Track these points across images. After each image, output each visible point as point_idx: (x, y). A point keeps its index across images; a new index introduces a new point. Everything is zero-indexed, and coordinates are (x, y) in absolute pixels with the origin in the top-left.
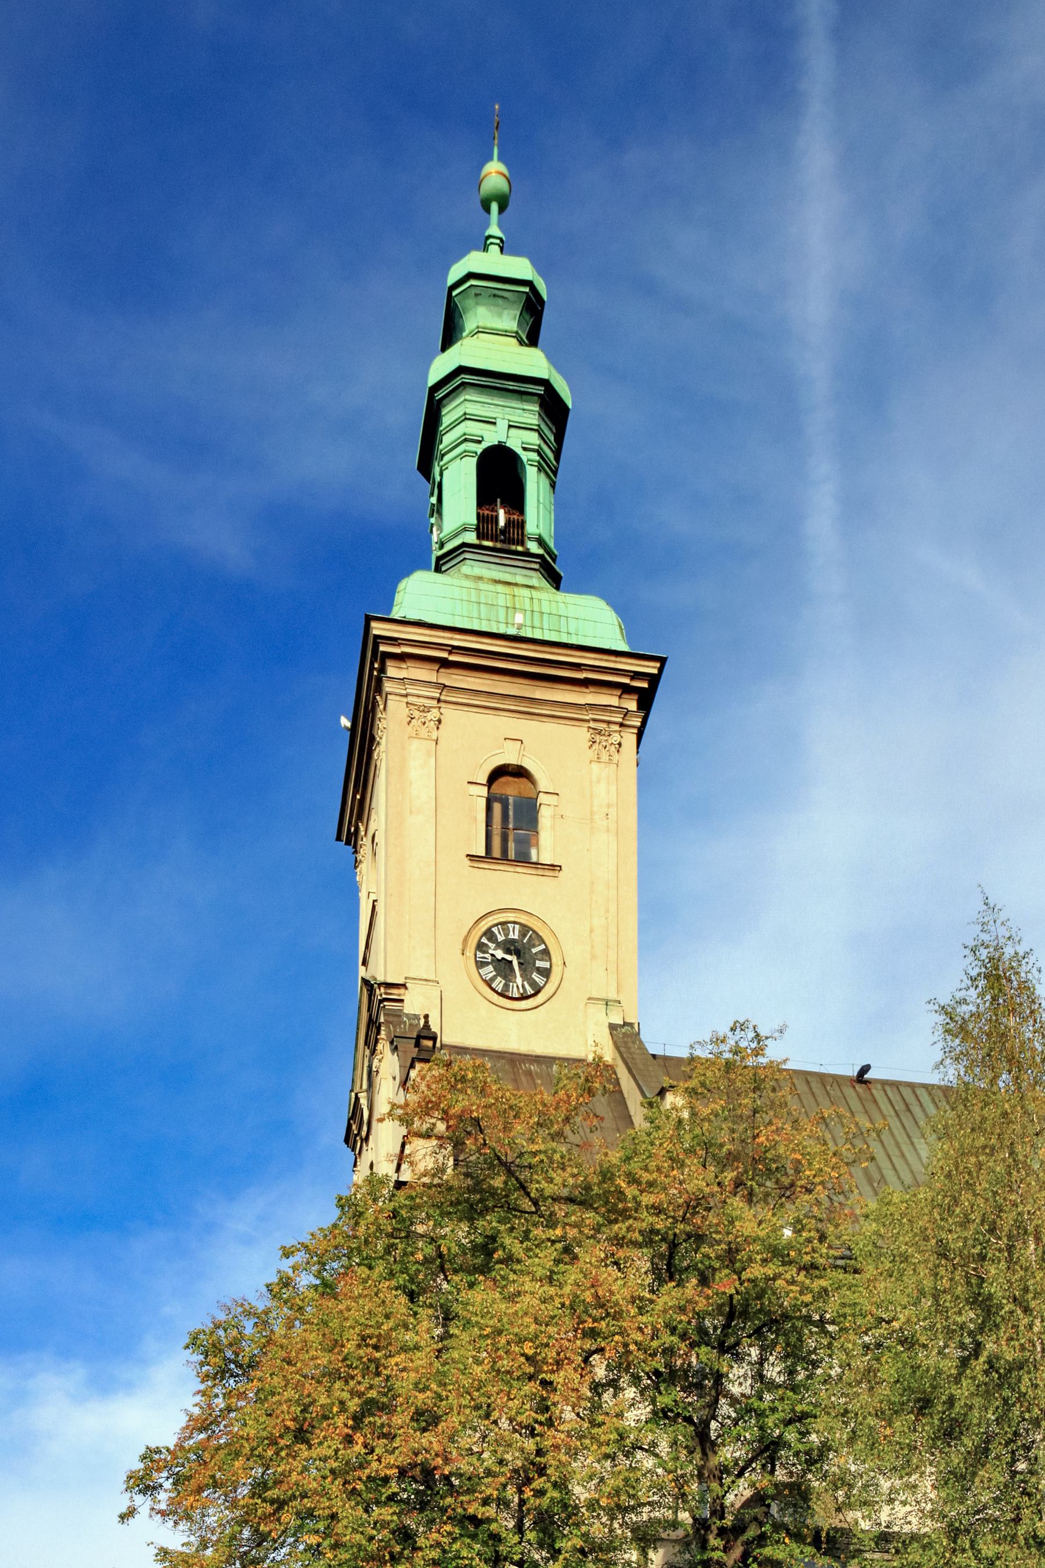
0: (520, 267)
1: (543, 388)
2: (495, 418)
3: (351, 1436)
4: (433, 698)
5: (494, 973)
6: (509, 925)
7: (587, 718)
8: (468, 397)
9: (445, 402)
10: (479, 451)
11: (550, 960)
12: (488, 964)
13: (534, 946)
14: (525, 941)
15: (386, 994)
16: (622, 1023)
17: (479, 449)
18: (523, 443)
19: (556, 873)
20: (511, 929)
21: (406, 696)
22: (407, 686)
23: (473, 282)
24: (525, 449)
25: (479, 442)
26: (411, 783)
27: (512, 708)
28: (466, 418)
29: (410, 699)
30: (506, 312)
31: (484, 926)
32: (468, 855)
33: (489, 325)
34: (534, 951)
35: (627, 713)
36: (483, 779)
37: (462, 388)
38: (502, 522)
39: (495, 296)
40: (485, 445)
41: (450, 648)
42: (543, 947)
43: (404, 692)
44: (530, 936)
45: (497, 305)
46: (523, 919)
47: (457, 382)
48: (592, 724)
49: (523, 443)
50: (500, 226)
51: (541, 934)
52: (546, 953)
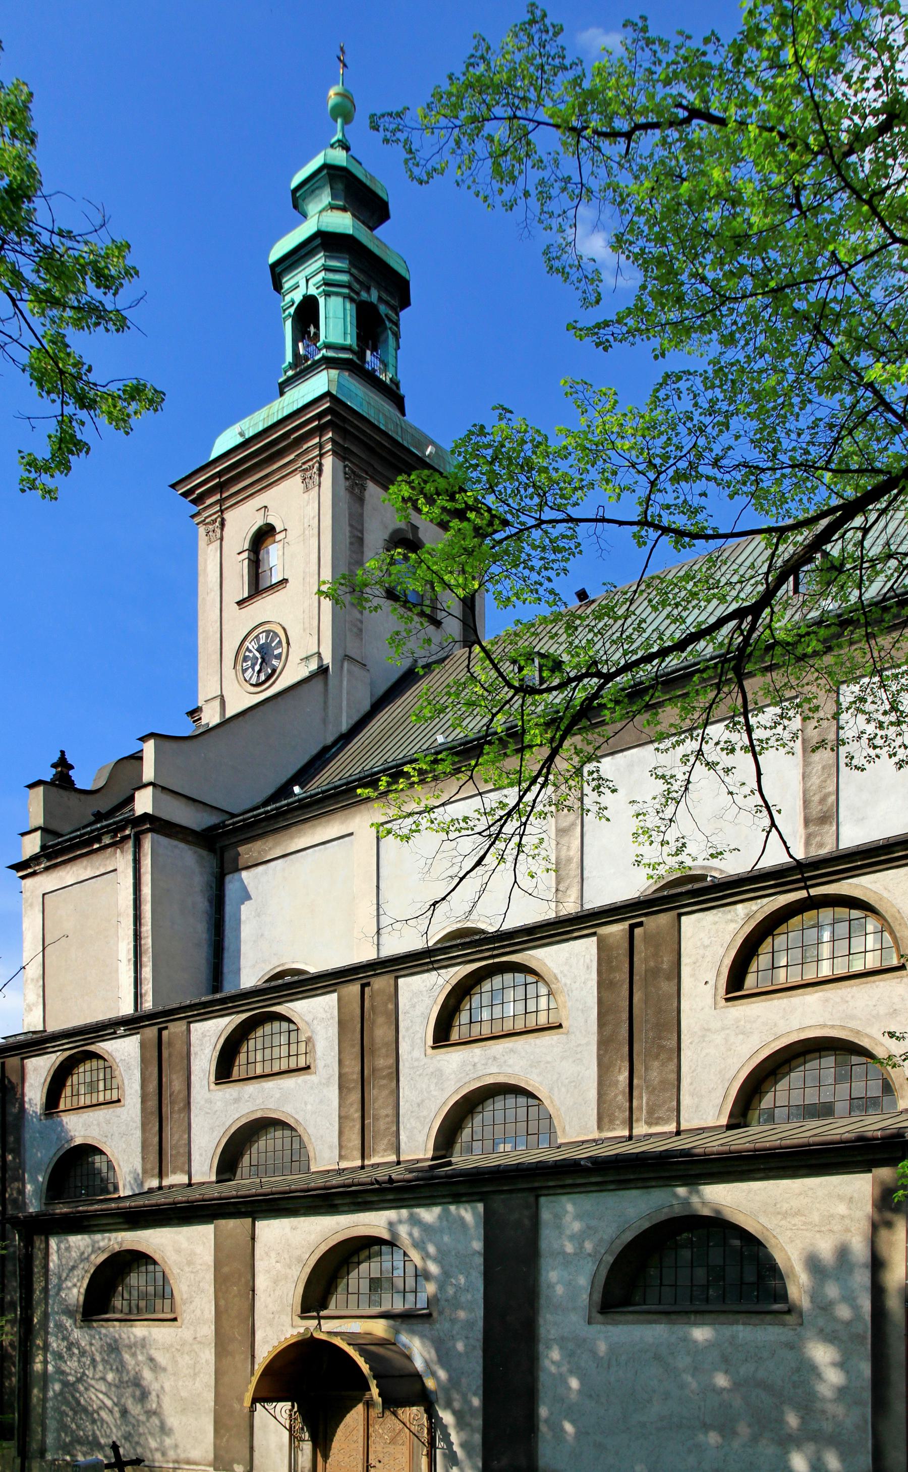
17: (292, 310)
46: (267, 627)
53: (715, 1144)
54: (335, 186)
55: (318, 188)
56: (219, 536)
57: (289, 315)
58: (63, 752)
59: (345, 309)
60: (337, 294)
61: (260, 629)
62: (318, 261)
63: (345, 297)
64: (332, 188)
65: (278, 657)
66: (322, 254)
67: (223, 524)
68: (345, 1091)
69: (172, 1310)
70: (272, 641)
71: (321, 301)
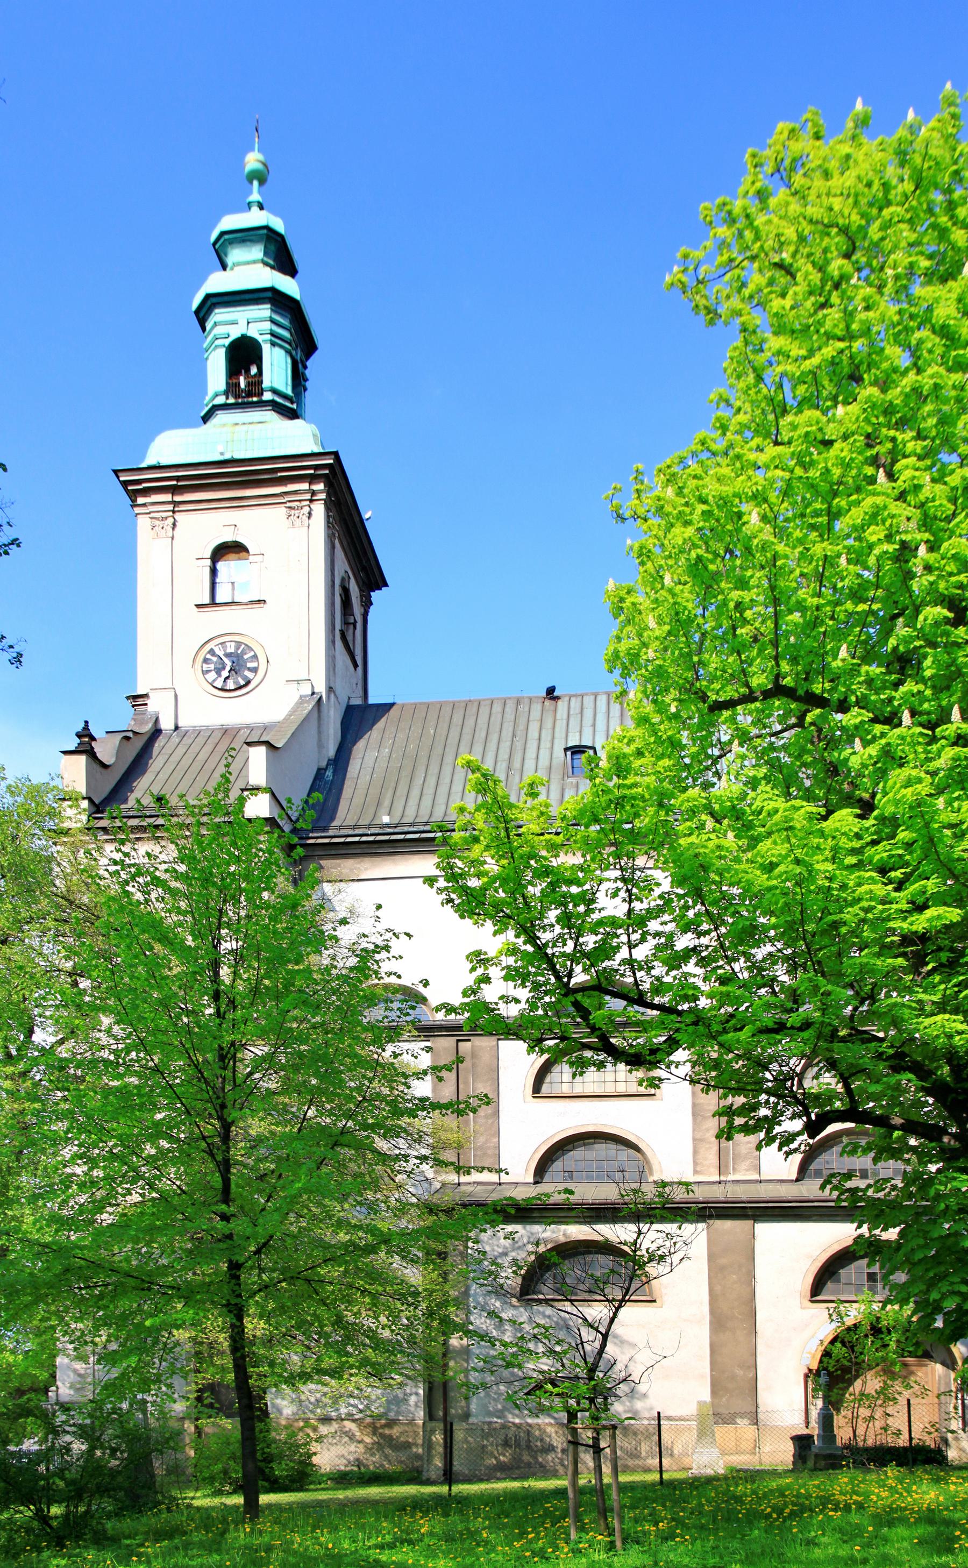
0: (255, 218)
16: (83, 759)
17: (227, 342)
23: (226, 237)
29: (152, 515)
31: (207, 648)
35: (314, 493)
38: (243, 385)
47: (209, 303)
48: (289, 504)
50: (259, 192)
52: (255, 657)
53: (520, 1194)
55: (251, 241)
58: (86, 722)
62: (264, 311)
63: (287, 352)
65: (255, 670)
68: (699, 1118)
69: (651, 1293)
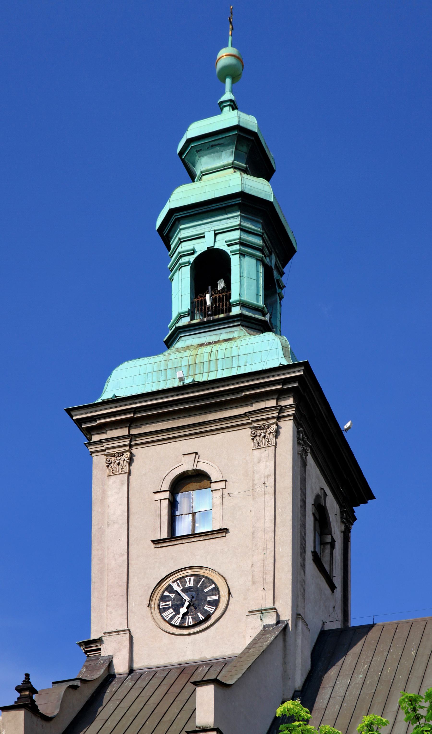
1: (240, 199)
2: (204, 233)
3: (416, 715)
4: (125, 446)
5: (174, 613)
6: (186, 578)
7: (249, 421)
8: (182, 227)
9: (171, 235)
10: (192, 261)
11: (219, 594)
12: (169, 608)
13: (206, 587)
14: (198, 586)
15: (87, 648)
17: (192, 259)
18: (226, 242)
19: (224, 534)
20: (188, 581)
21: (105, 450)
22: (104, 444)
24: (229, 245)
25: (192, 254)
26: (108, 506)
27: (188, 433)
28: (181, 241)
30: (224, 153)
32: (152, 541)
33: (209, 167)
34: (206, 591)
36: (166, 486)
37: (177, 222)
39: (212, 146)
40: (196, 255)
41: (133, 410)
42: (213, 586)
43: (103, 448)
44: (203, 581)
45: (217, 152)
46: (197, 572)
47: (173, 219)
49: (226, 242)
50: (233, 91)
51: (211, 578)
54: (240, 148)
56: (126, 469)
57: (189, 263)
58: (27, 675)
59: (257, 271)
60: (252, 256)
61: (187, 573)
63: (259, 260)
64: (236, 149)
65: (216, 603)
66: (238, 213)
67: (131, 460)
70: (204, 586)
71: (235, 260)
